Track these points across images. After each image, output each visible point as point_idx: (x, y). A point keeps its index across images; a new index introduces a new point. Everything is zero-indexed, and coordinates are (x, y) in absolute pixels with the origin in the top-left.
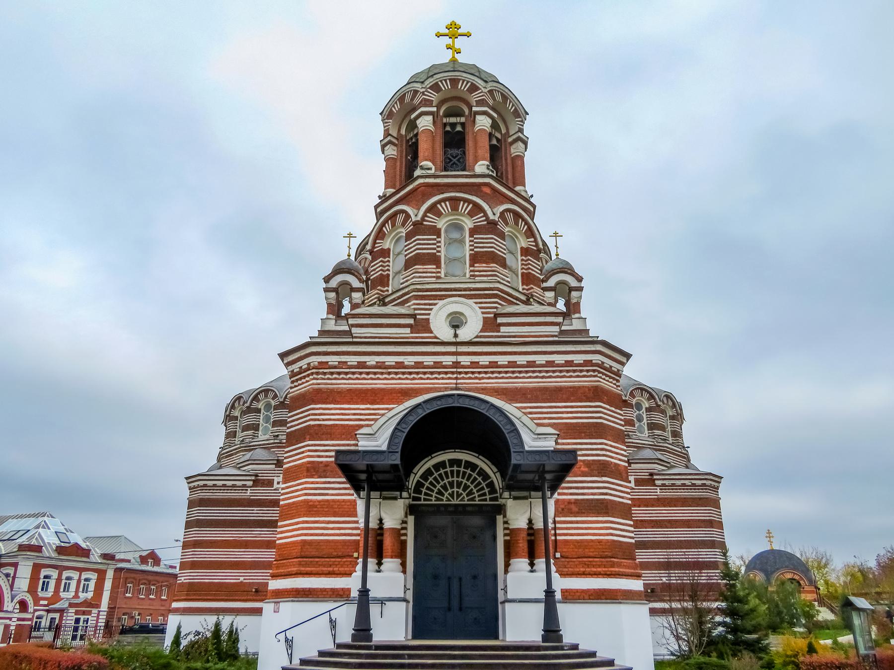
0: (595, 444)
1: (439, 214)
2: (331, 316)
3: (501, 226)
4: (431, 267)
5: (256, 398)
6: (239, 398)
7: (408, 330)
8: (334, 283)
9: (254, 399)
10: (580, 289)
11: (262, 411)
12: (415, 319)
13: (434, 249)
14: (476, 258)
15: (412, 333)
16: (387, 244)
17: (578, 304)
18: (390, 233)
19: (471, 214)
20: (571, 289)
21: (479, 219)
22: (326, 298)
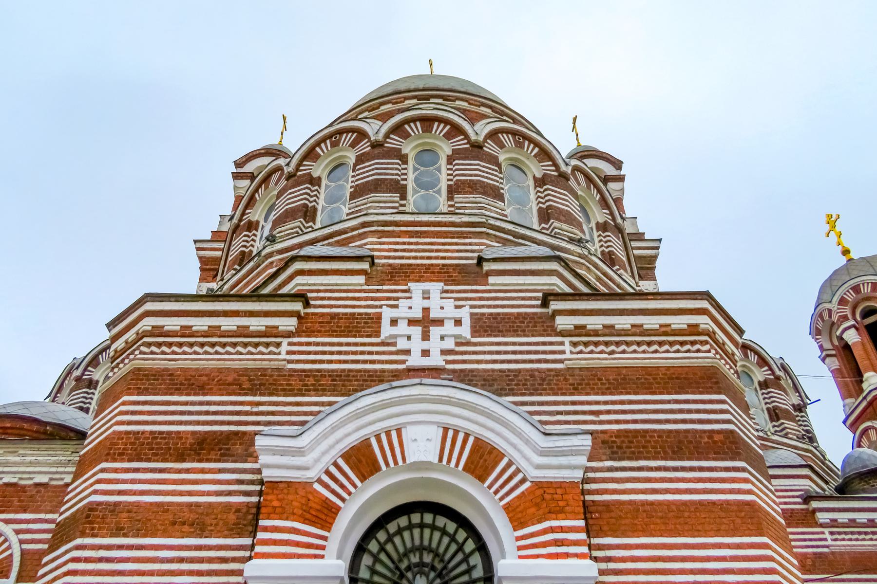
0: (711, 402)
1: (406, 136)
3: (490, 147)
4: (396, 197)
5: (310, 154)
7: (361, 279)
8: (250, 168)
10: (621, 179)
11: (324, 182)
12: (373, 264)
14: (452, 191)
15: (366, 284)
16: (318, 169)
18: (262, 200)
19: (448, 136)
20: (606, 180)
21: (460, 143)
22: (235, 188)
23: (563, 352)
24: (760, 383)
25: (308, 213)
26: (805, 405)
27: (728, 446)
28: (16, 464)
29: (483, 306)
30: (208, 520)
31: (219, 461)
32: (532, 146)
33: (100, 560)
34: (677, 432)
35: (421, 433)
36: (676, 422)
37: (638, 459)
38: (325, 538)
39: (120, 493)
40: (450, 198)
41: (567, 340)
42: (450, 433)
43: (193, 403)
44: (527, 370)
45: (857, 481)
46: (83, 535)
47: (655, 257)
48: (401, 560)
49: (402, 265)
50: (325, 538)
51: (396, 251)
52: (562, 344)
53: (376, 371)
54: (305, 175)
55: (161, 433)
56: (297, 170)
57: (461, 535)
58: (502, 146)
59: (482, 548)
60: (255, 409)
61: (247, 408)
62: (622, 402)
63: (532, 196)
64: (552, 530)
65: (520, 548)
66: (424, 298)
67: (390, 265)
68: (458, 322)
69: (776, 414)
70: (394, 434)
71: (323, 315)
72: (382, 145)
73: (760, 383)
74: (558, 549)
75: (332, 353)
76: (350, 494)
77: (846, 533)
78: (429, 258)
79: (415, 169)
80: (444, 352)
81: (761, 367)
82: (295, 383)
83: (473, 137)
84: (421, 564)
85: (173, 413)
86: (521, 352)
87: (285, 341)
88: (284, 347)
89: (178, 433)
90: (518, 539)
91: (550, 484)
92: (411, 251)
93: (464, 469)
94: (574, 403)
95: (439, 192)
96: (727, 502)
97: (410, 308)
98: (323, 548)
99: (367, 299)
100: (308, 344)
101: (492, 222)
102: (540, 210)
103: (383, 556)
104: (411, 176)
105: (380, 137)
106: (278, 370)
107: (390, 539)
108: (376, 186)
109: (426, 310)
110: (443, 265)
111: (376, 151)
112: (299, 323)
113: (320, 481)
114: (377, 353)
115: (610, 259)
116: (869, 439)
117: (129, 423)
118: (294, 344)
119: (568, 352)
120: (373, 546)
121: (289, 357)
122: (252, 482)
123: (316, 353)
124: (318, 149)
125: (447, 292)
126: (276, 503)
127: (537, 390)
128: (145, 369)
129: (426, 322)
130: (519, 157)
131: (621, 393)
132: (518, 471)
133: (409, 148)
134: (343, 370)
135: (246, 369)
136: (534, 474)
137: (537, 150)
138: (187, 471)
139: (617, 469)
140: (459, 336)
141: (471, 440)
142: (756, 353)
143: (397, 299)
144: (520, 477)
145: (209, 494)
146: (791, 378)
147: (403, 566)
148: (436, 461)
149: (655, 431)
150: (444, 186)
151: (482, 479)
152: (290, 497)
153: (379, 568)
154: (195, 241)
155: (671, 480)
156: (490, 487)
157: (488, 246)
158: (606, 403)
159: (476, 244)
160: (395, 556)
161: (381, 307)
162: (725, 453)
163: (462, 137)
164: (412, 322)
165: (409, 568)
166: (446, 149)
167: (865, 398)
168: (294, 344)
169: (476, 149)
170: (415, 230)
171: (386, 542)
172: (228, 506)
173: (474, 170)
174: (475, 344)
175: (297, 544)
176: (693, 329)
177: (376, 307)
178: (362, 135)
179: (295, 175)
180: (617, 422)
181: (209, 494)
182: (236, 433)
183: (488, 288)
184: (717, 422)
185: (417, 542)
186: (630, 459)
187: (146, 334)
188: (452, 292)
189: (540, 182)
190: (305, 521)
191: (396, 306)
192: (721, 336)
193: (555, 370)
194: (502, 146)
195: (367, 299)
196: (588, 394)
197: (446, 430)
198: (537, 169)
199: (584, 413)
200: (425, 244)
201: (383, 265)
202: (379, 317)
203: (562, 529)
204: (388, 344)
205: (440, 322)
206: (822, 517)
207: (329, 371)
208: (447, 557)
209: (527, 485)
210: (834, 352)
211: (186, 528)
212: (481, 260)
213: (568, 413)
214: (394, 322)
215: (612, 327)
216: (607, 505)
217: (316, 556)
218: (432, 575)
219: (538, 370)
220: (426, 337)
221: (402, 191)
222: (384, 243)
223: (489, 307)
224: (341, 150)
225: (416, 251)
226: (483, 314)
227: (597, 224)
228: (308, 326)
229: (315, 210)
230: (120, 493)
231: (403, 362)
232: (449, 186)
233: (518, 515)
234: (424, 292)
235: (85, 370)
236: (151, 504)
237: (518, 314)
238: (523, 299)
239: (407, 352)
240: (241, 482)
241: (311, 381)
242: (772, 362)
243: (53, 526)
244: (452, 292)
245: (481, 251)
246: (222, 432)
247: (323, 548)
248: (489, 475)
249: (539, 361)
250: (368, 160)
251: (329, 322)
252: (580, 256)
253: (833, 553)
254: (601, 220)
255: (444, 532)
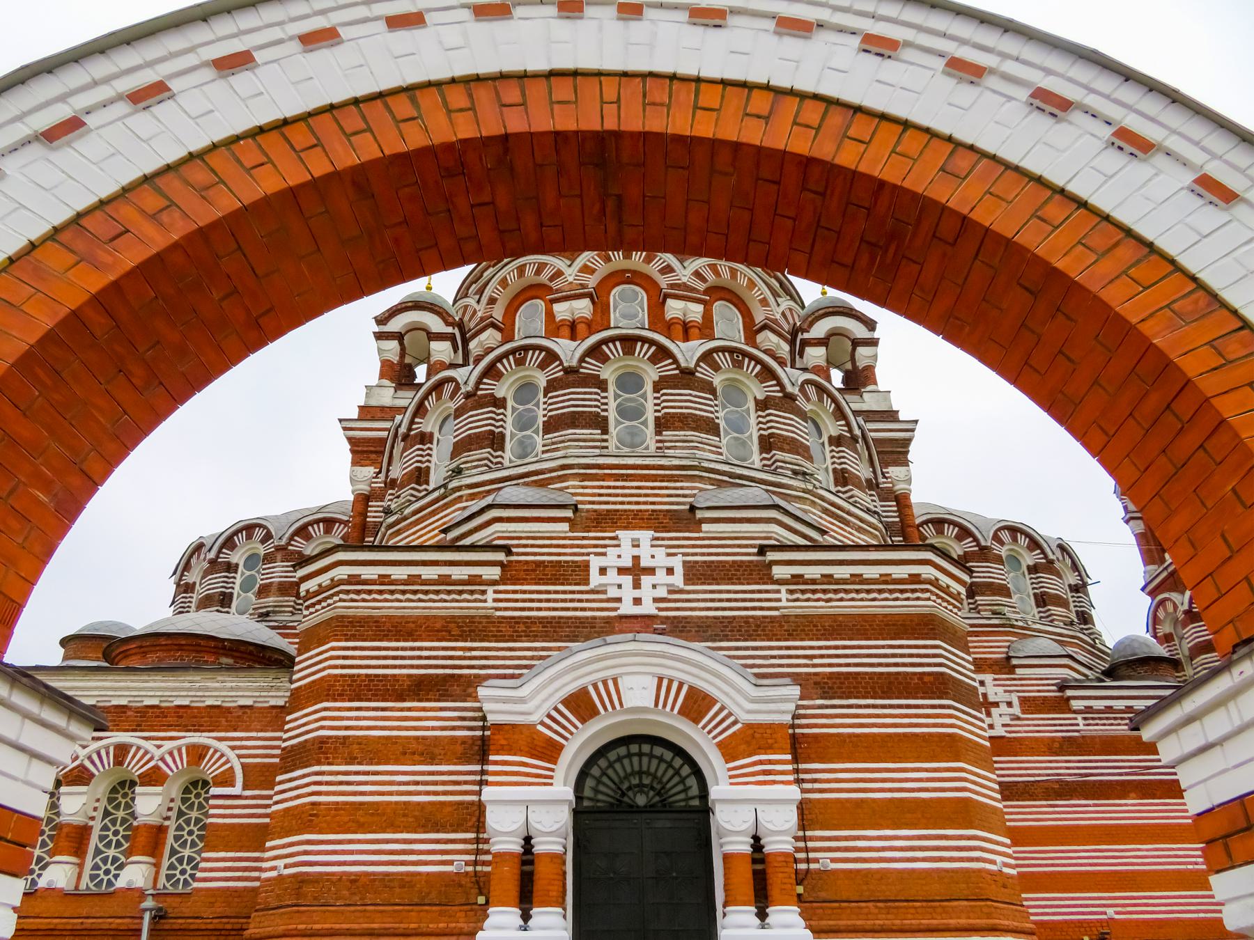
2: (386, 382)
3: (704, 372)
6: (198, 548)
7: (565, 527)
8: (396, 325)
9: (223, 546)
10: (874, 343)
13: (596, 406)
14: (662, 424)
17: (870, 369)
19: (654, 360)
20: (856, 343)
22: (379, 350)
23: (779, 600)
24: (1029, 567)
25: (496, 441)
26: (1085, 585)
27: (937, 686)
28: (216, 689)
29: (696, 554)
30: (436, 751)
31: (439, 701)
32: (753, 363)
33: (341, 783)
34: (889, 674)
35: (638, 683)
36: (888, 665)
37: (848, 698)
38: (552, 770)
39: (347, 728)
40: (658, 433)
41: (783, 588)
42: (665, 683)
43: (403, 649)
44: (742, 617)
45: (1124, 668)
46: (319, 763)
47: (909, 440)
48: (622, 782)
49: (608, 511)
50: (552, 770)
51: (600, 495)
52: (778, 591)
53: (587, 618)
54: (486, 395)
55: (376, 676)
56: (477, 388)
57: (678, 762)
58: (716, 368)
59: (697, 772)
60: (468, 654)
61: (460, 653)
62: (836, 648)
63: (753, 420)
64: (761, 762)
65: (731, 777)
66: (634, 546)
67: (595, 511)
68: (670, 571)
69: (1044, 601)
70: (611, 683)
71: (527, 562)
72: (577, 371)
73: (1029, 567)
74: (767, 776)
75: (540, 601)
76: (572, 734)
77: (1100, 719)
78: (638, 503)
79: (616, 396)
80: (656, 600)
81: (1032, 551)
82: (505, 629)
83: (683, 364)
84: (641, 786)
85: (385, 658)
86: (736, 600)
87: (490, 589)
88: (490, 595)
89: (395, 676)
90: (729, 770)
91: (760, 725)
92: (617, 495)
93: (679, 713)
94: (788, 648)
95: (645, 423)
96: (930, 734)
97: (619, 556)
98: (551, 777)
99: (572, 546)
100: (515, 592)
101: (705, 464)
102: (761, 437)
103: (605, 779)
104: (612, 405)
105: (574, 363)
106: (487, 617)
107: (611, 765)
108: (574, 420)
109: (636, 559)
110: (653, 511)
111: (571, 378)
112: (503, 571)
113: (542, 723)
114: (588, 601)
115: (842, 478)
116: (1165, 609)
117: (343, 667)
118: (500, 592)
119: (784, 600)
120: (595, 771)
121: (496, 605)
122: (474, 719)
123: (524, 601)
124: (499, 365)
125: (657, 539)
126: (503, 742)
127: (750, 635)
128: (348, 617)
129: (636, 571)
130: (737, 377)
131: (836, 639)
132: (730, 714)
133: (608, 373)
134: (554, 618)
135: (453, 617)
136: (745, 717)
137: (759, 367)
138: (409, 709)
139: (827, 707)
140: (672, 585)
141: (685, 689)
142: (1027, 535)
143: (605, 546)
144: (732, 719)
145: (433, 728)
146: (1070, 557)
147: (625, 786)
148: (652, 706)
149: (866, 673)
150: (650, 416)
151: (696, 721)
152: (516, 737)
153: (602, 788)
154: (340, 420)
155: (878, 716)
156: (704, 728)
157: (701, 490)
158: (820, 648)
159: (687, 488)
160: (616, 780)
161: (588, 554)
162: (933, 693)
163: (670, 361)
164: (622, 571)
165: (629, 788)
166: (651, 374)
167: (1166, 569)
168: (500, 592)
169: (686, 378)
170: (622, 474)
171: (607, 768)
172: (453, 738)
173: (685, 401)
174: (689, 592)
175: (527, 775)
176: (915, 579)
177: (583, 554)
178: (552, 356)
179: (475, 394)
180: (830, 665)
181: (433, 728)
182: (453, 676)
183: (701, 535)
184: (929, 665)
185: (636, 768)
186: (841, 698)
187: (341, 582)
188: (663, 539)
189: (762, 405)
190: (532, 756)
191: (604, 554)
192: (945, 580)
193: (771, 617)
194: (716, 368)
195: (572, 546)
196: (802, 640)
197: (660, 679)
198: (758, 391)
199: (798, 657)
200: (632, 488)
201: (588, 511)
202: (586, 565)
203: (770, 762)
204: (598, 592)
205: (651, 571)
206: (1075, 704)
207: (539, 618)
208: (665, 780)
209: (738, 726)
210: (1139, 515)
211: (416, 757)
212: (693, 509)
213: (782, 657)
214: (603, 571)
215: (831, 576)
216: (815, 736)
217: (545, 784)
218: (651, 793)
219: (752, 617)
220: (637, 585)
221: (601, 424)
222: (586, 487)
223: (703, 554)
224: (527, 369)
225: (623, 495)
226: (696, 562)
227: (830, 438)
228: (511, 573)
229: (502, 436)
230: (347, 728)
231: (616, 609)
232: (657, 418)
233: (729, 750)
234: (633, 540)
235: (220, 552)
236: (380, 737)
237: (734, 562)
238: (739, 546)
239: (619, 600)
240: (463, 719)
241: (522, 628)
242: (1045, 545)
243: (278, 752)
244: (663, 539)
245: (694, 496)
246: (437, 675)
247: (551, 777)
248: (703, 717)
249: (754, 609)
250: (562, 388)
251: (534, 570)
252: (804, 491)
253: (1083, 737)
254: (834, 433)
255: (661, 759)
